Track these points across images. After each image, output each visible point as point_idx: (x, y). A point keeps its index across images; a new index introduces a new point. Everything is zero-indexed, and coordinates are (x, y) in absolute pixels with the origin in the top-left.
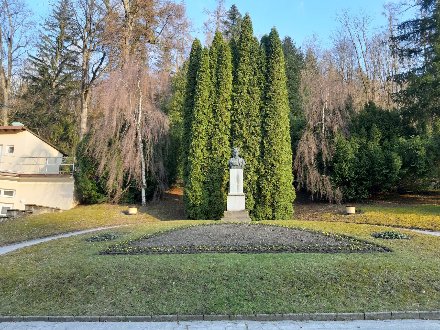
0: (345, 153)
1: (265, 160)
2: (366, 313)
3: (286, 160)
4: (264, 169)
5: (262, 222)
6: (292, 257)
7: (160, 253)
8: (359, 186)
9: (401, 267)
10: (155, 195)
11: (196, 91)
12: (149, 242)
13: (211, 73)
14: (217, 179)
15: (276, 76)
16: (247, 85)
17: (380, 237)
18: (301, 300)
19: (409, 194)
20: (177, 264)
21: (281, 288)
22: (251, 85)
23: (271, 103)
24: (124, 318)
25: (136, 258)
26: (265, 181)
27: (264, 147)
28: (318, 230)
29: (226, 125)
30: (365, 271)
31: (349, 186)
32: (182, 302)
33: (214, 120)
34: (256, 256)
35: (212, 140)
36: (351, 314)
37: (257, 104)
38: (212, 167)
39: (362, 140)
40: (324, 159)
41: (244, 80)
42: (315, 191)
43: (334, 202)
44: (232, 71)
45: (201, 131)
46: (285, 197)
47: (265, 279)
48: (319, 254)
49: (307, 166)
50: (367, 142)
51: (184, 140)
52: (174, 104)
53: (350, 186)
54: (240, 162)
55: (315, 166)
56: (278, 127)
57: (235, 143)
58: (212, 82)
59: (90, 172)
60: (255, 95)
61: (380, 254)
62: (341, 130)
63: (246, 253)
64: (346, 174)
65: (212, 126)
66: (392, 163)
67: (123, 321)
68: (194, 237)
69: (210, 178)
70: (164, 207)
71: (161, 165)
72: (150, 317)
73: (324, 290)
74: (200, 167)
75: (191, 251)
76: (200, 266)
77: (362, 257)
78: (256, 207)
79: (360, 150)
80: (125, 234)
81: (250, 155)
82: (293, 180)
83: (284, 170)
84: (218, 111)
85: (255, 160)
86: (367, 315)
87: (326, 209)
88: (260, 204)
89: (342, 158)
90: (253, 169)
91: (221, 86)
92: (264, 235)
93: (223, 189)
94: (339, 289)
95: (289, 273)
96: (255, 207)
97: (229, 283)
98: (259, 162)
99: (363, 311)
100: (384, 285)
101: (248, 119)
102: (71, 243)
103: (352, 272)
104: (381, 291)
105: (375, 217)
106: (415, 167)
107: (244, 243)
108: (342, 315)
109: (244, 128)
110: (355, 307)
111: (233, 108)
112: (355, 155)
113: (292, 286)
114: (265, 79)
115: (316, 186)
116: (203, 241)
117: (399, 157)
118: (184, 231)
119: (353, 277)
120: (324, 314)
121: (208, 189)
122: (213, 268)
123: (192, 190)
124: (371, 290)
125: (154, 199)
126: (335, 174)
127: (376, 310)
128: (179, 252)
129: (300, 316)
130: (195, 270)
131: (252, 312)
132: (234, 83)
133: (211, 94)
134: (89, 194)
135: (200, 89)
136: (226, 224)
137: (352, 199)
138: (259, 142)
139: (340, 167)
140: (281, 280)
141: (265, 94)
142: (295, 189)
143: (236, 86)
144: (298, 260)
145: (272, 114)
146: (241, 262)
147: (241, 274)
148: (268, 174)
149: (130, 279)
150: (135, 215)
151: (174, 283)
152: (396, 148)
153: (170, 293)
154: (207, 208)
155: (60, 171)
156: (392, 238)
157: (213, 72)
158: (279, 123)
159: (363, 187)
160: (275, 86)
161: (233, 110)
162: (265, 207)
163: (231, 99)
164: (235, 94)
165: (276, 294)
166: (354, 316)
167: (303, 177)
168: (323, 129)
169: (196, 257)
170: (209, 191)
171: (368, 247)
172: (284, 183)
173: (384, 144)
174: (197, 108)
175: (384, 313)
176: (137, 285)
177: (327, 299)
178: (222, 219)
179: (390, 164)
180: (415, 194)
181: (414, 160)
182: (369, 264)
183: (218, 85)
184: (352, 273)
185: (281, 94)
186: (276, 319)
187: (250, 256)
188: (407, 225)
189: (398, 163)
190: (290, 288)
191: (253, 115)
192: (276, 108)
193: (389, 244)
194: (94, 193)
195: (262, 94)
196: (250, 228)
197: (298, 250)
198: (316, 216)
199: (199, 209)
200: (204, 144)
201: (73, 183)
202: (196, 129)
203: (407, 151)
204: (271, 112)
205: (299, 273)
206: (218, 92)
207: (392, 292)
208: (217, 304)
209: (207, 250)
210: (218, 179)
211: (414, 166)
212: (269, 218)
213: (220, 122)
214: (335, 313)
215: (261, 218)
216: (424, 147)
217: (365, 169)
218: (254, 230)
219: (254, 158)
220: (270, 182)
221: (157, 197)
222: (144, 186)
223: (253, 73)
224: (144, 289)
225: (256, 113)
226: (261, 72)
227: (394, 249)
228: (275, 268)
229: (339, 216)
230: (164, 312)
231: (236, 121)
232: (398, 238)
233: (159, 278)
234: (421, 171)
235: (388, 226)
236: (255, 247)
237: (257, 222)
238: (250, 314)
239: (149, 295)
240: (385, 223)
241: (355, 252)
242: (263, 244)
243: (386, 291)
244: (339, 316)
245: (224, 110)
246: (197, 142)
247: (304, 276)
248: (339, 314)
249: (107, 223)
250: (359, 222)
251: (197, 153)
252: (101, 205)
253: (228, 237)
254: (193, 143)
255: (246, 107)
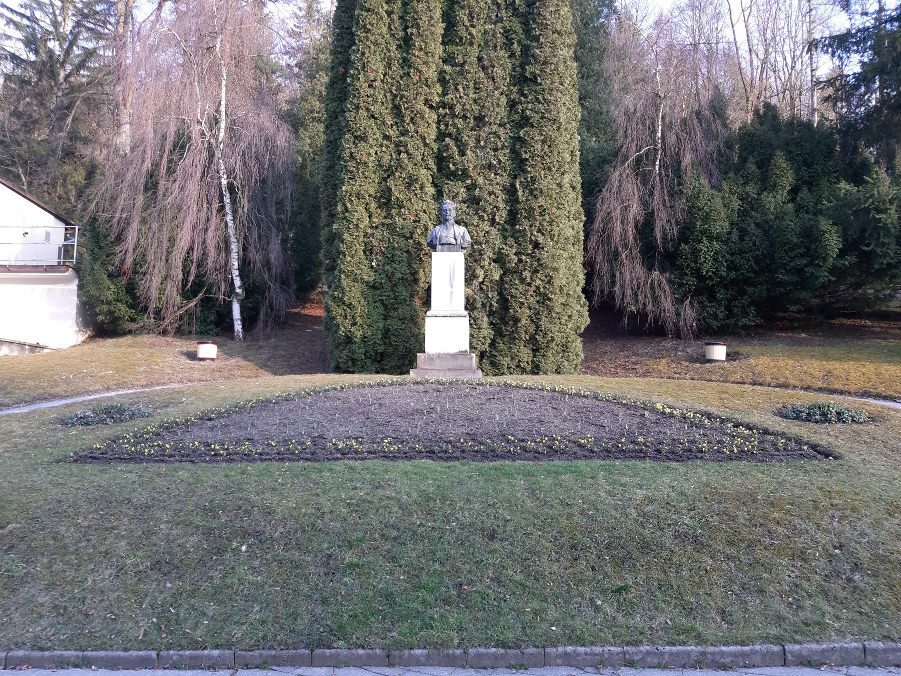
0: (707, 218)
1: (519, 231)
2: (789, 647)
3: (569, 233)
4: (516, 254)
5: (509, 379)
6: (576, 472)
7: (230, 458)
8: (735, 298)
9: (872, 504)
10: (262, 316)
11: (353, 57)
12: (212, 429)
13: (389, 13)
14: (402, 279)
15: (549, 23)
16: (480, 45)
17: (797, 418)
18: (599, 602)
19: (845, 318)
20: (263, 493)
21: (545, 565)
22: (489, 46)
23: (536, 91)
24: (77, 656)
25: (159, 475)
26: (517, 282)
27: (517, 201)
28: (643, 398)
29: (426, 145)
30: (776, 515)
31: (712, 298)
32: (257, 608)
33: (397, 132)
34: (482, 468)
35: (392, 182)
36: (746, 648)
37: (502, 94)
38: (391, 248)
39: (748, 188)
40: (658, 234)
41: (470, 34)
42: (634, 308)
43: (678, 335)
44: (443, 11)
45: (364, 158)
46: (563, 321)
47: (499, 536)
48: (648, 464)
49: (617, 249)
50: (759, 194)
51: (326, 184)
52: (314, 104)
53: (715, 298)
54: (457, 234)
55: (636, 251)
56: (551, 152)
57: (447, 190)
58: (393, 35)
59: (111, 260)
60: (498, 71)
61: (808, 465)
62: (700, 164)
63: (457, 458)
64: (707, 268)
65: (392, 146)
66: (818, 243)
67: (76, 666)
68: (330, 417)
69: (387, 275)
70: (285, 344)
71: (275, 246)
72: (154, 654)
73: (665, 573)
74: (363, 248)
75: (313, 453)
76: (322, 500)
77: (763, 473)
78: (494, 345)
79: (743, 213)
80: (167, 406)
81: (484, 220)
82: (583, 282)
83: (564, 256)
84: (406, 109)
85: (494, 231)
86: (791, 652)
87: (658, 350)
88: (504, 337)
89: (701, 232)
90: (489, 254)
91: (415, 46)
92: (506, 412)
93: (417, 303)
94: (706, 570)
95: (567, 519)
96: (493, 344)
97: (397, 549)
98: (505, 238)
99: (779, 640)
100: (831, 555)
101: (480, 130)
102: (17, 427)
103: (742, 516)
104: (826, 576)
105: (774, 367)
106: (870, 251)
107: (454, 431)
108: (718, 653)
109: (469, 152)
110: (755, 626)
111: (443, 102)
112: (732, 224)
113: (575, 559)
114: (523, 30)
115: (637, 296)
116: (351, 427)
117: (835, 228)
118: (309, 400)
119: (744, 532)
120: (668, 648)
121: (382, 301)
122: (358, 505)
123: (344, 303)
124: (797, 573)
125: (260, 325)
126: (683, 269)
127: (817, 637)
128: (281, 457)
129: (596, 654)
130: (309, 511)
131: (456, 642)
132: (446, 40)
133: (389, 66)
134: (111, 313)
135: (363, 54)
136: (417, 383)
137: (718, 327)
138: (506, 189)
139: (695, 253)
140: (544, 542)
141: (523, 68)
142: (588, 303)
143: (450, 48)
144: (590, 481)
145: (537, 117)
146: (439, 486)
147: (435, 521)
148: (524, 266)
149: (123, 536)
150: (212, 362)
151: (244, 548)
152: (828, 209)
153: (228, 581)
154: (380, 345)
155: (59, 258)
156: (829, 421)
157: (396, 10)
158: (554, 142)
159: (746, 300)
160: (548, 50)
161: (444, 108)
162: (515, 344)
163: (439, 80)
164: (448, 68)
165: (528, 584)
166: (753, 657)
167: (607, 277)
168: (657, 163)
169: (321, 471)
170: (386, 307)
171: (774, 444)
172: (561, 289)
173: (798, 199)
174: (355, 101)
175: (841, 648)
176: (140, 553)
177: (673, 602)
178: (412, 372)
179: (813, 246)
180: (858, 318)
181: (871, 235)
182: (787, 494)
183: (406, 43)
184: (742, 520)
185: (561, 68)
186: (526, 663)
187: (462, 469)
188: (852, 388)
189: (833, 242)
190: (568, 565)
191: (492, 121)
192: (548, 102)
193: (825, 437)
194: (122, 309)
195: (514, 69)
196: (474, 394)
197: (592, 451)
198: (634, 366)
199: (359, 348)
200: (372, 191)
201: (74, 286)
202: (351, 153)
203: (855, 213)
204: (536, 113)
205: (593, 519)
206: (406, 62)
207: (857, 577)
208: (356, 616)
209: (356, 452)
210: (405, 277)
211: (870, 248)
212: (524, 371)
213: (412, 136)
214: (697, 644)
215: (506, 371)
216: (895, 205)
217: (753, 257)
218: (484, 398)
219: (492, 228)
220: (529, 284)
221: (266, 321)
222: (237, 294)
223: (494, 17)
224: (156, 566)
225: (499, 117)
226: (513, 14)
227: (843, 452)
228: (529, 504)
229: (687, 366)
230: (197, 642)
231: (450, 135)
232: (844, 422)
233: (203, 534)
234: (885, 262)
235: (807, 388)
236: (481, 443)
237: (494, 380)
238: (448, 648)
239: (168, 585)
240: (798, 383)
241: (740, 459)
242: (503, 436)
243: (838, 575)
244: (709, 656)
245: (420, 106)
246: (354, 185)
247: (607, 529)
248: (711, 649)
249: (138, 380)
250: (736, 381)
251: (355, 214)
252: (139, 339)
253: (416, 417)
254: (344, 188)
255: (475, 101)
